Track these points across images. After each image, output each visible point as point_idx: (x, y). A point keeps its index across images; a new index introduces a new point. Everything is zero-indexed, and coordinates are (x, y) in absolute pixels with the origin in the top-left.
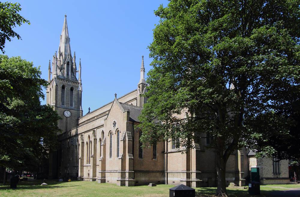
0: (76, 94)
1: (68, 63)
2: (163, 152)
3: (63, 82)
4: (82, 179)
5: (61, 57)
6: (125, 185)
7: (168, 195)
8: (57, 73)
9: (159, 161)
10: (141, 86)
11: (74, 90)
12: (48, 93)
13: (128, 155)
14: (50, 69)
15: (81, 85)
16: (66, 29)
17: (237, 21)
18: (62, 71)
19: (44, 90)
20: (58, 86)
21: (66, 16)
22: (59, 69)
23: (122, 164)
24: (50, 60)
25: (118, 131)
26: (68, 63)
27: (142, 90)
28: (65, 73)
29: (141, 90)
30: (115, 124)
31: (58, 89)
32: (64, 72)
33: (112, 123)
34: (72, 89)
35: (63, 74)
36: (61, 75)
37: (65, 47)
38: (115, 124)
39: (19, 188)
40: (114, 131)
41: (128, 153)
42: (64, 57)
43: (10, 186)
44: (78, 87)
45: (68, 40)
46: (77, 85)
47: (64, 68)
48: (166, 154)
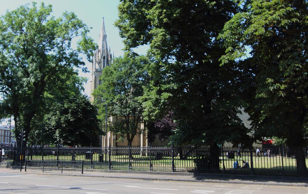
1: (104, 57)
3: (100, 74)
4: (250, 125)
5: (100, 52)
8: (95, 67)
9: (136, 139)
12: (91, 82)
14: (40, 174)
16: (104, 28)
18: (100, 64)
19: (85, 85)
20: (97, 77)
21: (103, 18)
22: (98, 63)
26: (104, 57)
28: (102, 65)
31: (97, 80)
32: (101, 65)
35: (100, 67)
36: (99, 68)
37: (103, 44)
39: (31, 164)
42: (101, 52)
43: (281, 112)
45: (105, 37)
47: (101, 62)
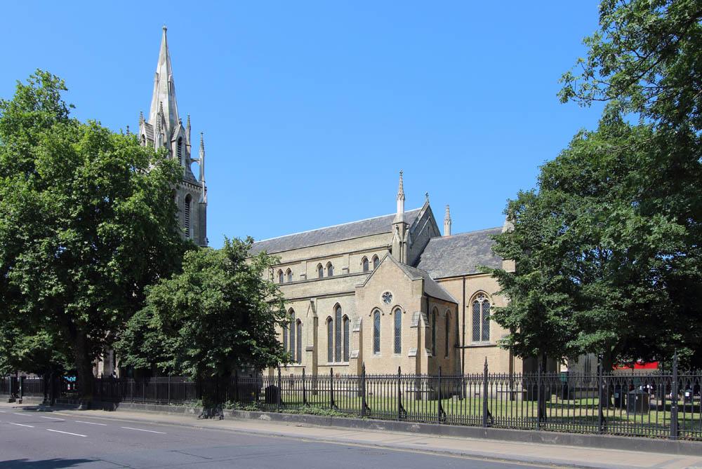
0: (196, 210)
2: (457, 346)
6: (329, 361)
7: (696, 459)
10: (401, 226)
11: (193, 200)
13: (425, 351)
15: (205, 190)
17: (671, 99)
23: (314, 334)
24: (128, 127)
25: (397, 310)
27: (404, 234)
29: (401, 234)
30: (387, 297)
33: (382, 295)
34: (188, 200)
38: (387, 297)
40: (386, 308)
41: (426, 347)
44: (199, 195)
46: (197, 191)
48: (461, 350)
